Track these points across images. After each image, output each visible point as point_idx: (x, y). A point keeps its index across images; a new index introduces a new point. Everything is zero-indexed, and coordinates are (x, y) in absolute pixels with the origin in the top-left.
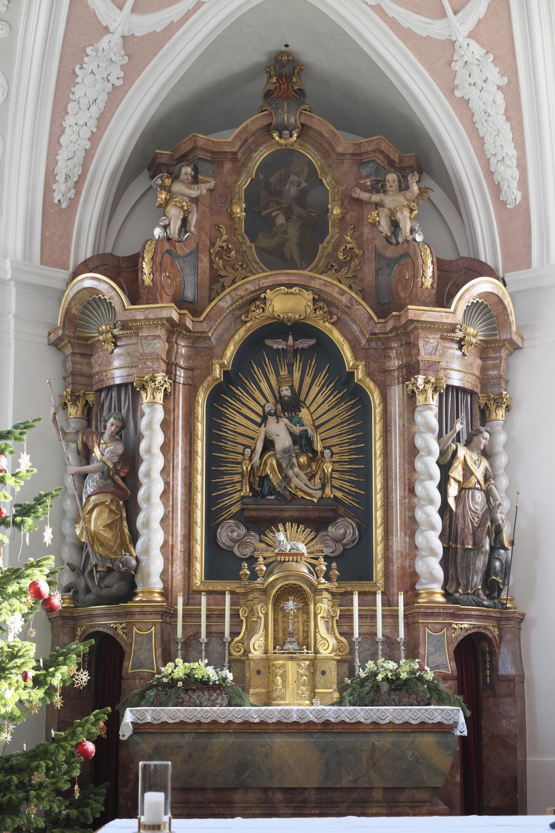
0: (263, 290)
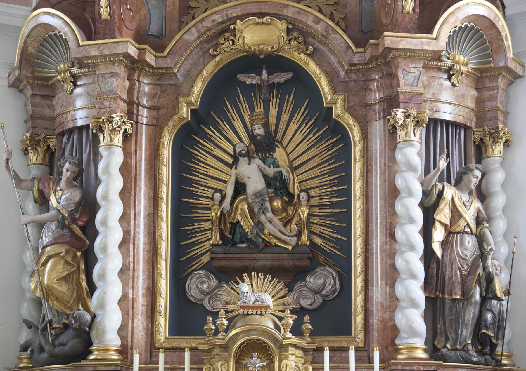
0: (233, 20)
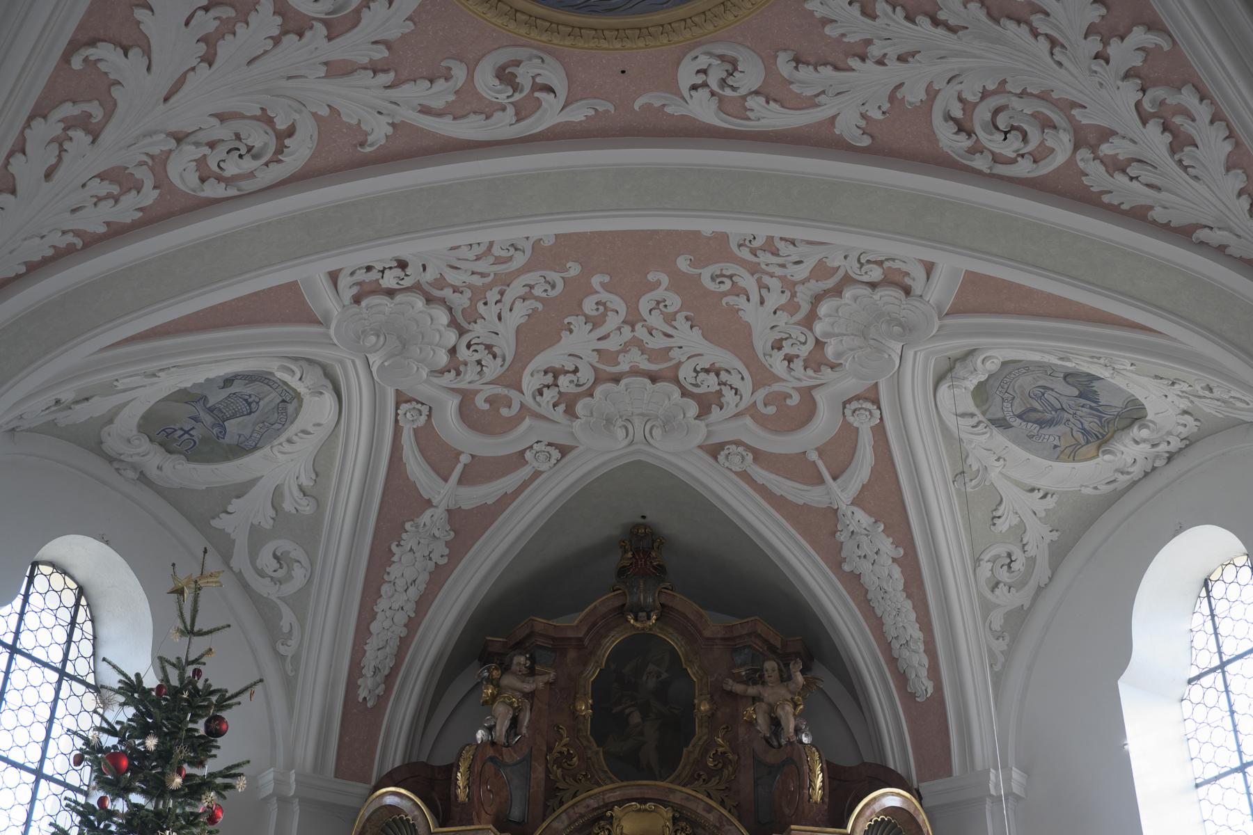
0: (610, 806)
